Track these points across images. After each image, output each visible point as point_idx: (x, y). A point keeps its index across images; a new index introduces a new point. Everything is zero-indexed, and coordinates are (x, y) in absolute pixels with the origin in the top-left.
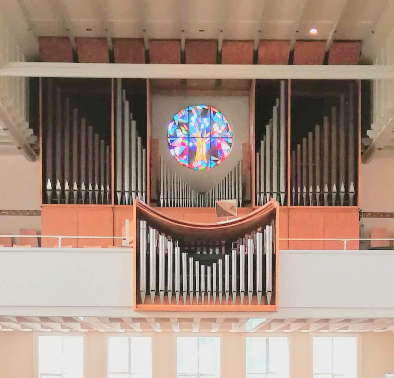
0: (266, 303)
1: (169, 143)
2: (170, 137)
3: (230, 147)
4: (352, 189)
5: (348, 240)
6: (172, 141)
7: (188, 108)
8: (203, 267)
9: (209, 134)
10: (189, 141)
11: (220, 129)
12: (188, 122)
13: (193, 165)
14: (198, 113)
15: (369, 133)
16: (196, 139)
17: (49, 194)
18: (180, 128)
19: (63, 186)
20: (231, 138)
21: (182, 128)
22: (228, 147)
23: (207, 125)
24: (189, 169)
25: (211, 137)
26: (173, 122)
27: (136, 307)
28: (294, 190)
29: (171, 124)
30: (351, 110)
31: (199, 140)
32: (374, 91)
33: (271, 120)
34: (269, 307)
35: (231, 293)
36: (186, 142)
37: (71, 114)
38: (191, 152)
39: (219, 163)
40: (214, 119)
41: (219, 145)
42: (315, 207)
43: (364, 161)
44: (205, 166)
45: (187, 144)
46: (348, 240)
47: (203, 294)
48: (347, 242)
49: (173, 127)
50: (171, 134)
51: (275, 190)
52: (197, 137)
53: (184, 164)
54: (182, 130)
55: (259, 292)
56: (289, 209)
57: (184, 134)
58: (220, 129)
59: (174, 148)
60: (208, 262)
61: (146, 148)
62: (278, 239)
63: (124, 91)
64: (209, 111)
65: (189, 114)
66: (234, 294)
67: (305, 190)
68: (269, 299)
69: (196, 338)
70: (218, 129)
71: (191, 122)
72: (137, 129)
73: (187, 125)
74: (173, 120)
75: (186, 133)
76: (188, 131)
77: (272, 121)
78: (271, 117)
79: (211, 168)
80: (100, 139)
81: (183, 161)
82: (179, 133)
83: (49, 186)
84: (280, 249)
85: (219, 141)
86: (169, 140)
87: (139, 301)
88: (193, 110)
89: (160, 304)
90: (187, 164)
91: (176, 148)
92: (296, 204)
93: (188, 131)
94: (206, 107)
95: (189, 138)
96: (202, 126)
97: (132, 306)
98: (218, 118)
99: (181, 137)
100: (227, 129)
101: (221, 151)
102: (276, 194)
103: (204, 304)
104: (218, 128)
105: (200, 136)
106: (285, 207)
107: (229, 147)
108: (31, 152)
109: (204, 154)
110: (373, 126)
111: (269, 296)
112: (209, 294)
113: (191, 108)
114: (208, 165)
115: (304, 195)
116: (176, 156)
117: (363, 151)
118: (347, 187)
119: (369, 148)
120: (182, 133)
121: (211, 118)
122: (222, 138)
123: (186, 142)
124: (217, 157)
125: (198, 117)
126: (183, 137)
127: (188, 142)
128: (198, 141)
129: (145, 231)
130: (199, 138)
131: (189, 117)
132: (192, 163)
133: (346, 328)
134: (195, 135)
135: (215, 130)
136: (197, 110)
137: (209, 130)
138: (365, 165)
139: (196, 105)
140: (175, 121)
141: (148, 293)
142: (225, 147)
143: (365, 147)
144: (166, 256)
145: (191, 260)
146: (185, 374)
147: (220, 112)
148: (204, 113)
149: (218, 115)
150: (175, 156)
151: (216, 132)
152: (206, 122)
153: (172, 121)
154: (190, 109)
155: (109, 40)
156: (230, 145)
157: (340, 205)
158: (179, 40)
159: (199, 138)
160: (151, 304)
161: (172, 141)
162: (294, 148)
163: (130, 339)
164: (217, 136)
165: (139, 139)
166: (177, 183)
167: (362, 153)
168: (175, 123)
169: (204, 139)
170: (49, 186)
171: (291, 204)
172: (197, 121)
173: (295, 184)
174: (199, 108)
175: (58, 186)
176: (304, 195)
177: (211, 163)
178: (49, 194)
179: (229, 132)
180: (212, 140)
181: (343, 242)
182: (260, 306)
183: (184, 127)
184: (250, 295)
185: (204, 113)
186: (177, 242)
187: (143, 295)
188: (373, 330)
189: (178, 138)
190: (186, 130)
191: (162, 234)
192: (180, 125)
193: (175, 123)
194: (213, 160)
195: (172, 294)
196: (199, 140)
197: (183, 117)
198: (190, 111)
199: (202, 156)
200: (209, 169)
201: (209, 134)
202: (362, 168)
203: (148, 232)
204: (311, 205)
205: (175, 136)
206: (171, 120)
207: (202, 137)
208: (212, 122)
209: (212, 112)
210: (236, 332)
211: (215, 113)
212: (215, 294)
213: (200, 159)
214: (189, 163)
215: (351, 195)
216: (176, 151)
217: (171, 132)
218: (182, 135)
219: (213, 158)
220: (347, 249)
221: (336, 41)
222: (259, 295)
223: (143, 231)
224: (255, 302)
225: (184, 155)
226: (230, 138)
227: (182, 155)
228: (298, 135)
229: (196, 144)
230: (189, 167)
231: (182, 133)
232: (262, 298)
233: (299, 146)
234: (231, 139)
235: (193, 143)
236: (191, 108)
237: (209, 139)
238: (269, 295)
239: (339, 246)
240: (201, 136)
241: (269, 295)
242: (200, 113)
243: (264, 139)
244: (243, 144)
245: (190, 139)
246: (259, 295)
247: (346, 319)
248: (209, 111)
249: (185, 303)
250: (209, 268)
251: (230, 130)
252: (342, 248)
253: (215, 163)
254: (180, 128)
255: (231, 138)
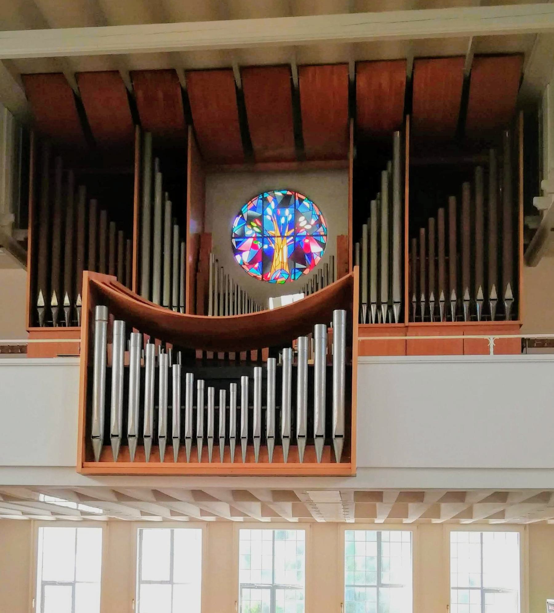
0: (333, 460)
1: (233, 246)
2: (234, 238)
3: (324, 250)
4: (509, 294)
5: (497, 337)
6: (238, 243)
7: (263, 196)
8: (211, 391)
9: (293, 230)
10: (263, 243)
11: (308, 223)
12: (263, 215)
13: (269, 276)
14: (276, 203)
15: (537, 202)
16: (273, 239)
17: (41, 312)
18: (250, 224)
19: (61, 300)
20: (324, 235)
21: (253, 224)
22: (321, 249)
23: (290, 218)
24: (263, 282)
25: (295, 235)
26: (241, 216)
27: (83, 467)
28: (414, 299)
29: (238, 219)
30: (507, 168)
31: (278, 240)
32: (544, 155)
33: (378, 193)
34: (338, 466)
35: (259, 441)
36: (259, 244)
37: (76, 191)
38: (265, 258)
39: (307, 272)
40: (300, 209)
41: (308, 246)
42: (449, 323)
43: (529, 262)
44: (286, 276)
45: (259, 247)
46: (497, 337)
47: (210, 442)
48: (496, 341)
49: (239, 224)
50: (236, 232)
51: (384, 298)
52: (275, 237)
53: (255, 275)
54: (252, 227)
55: (318, 438)
56: (407, 327)
57: (256, 232)
58: (308, 223)
59: (241, 252)
60: (220, 383)
61: (185, 241)
62: (357, 338)
63: (157, 160)
64: (293, 197)
65: (263, 204)
66: (271, 443)
67: (432, 298)
68: (339, 451)
69: (271, 531)
70: (305, 224)
71: (267, 214)
72: (173, 214)
73: (261, 219)
74: (240, 213)
75: (258, 230)
76: (262, 227)
77: (381, 195)
78: (379, 189)
79: (294, 279)
80: (118, 229)
81: (254, 271)
82: (249, 232)
83: (41, 301)
84: (359, 355)
85: (307, 241)
86: (234, 241)
87: (89, 455)
88: (270, 198)
89: (130, 462)
90: (260, 277)
91: (244, 254)
92: (418, 320)
93: (262, 227)
94: (289, 193)
95: (263, 237)
96: (283, 221)
97: (75, 465)
98: (305, 206)
99: (251, 237)
100: (319, 223)
101: (310, 255)
102: (386, 306)
103: (212, 462)
104: (305, 222)
105: (279, 235)
106: (401, 325)
107: (321, 249)
108: (18, 251)
109: (285, 260)
110: (544, 185)
111: (339, 446)
112: (222, 441)
113: (266, 195)
114: (290, 275)
115: (432, 305)
116: (244, 264)
117: (526, 243)
118: (501, 293)
119: (537, 233)
120: (253, 230)
121: (295, 208)
122: (312, 236)
123: (259, 244)
124: (305, 265)
125: (278, 206)
126: (254, 236)
127: (261, 244)
128: (276, 241)
129: (104, 324)
130: (278, 237)
131: (263, 207)
132: (268, 273)
133: (501, 515)
134: (272, 233)
135: (301, 225)
136: (275, 198)
137: (293, 225)
138: (529, 268)
139: (273, 191)
140: (243, 216)
141: (107, 441)
142: (315, 249)
143: (529, 233)
144: (143, 370)
145: (189, 377)
146: (253, 585)
147: (309, 199)
148: (286, 201)
149: (306, 203)
150: (242, 264)
151: (303, 228)
152: (288, 213)
153: (238, 216)
154: (265, 196)
155: (125, 76)
156: (323, 245)
157: (489, 319)
158: (229, 69)
159: (278, 237)
160: (112, 461)
161: (238, 243)
162: (414, 234)
163: (172, 532)
164: (304, 233)
165: (176, 228)
166: (234, 294)
167: (526, 246)
168: (243, 218)
169: (285, 238)
170: (41, 301)
171: (410, 320)
172: (275, 212)
173: (416, 289)
174: (279, 194)
175: (54, 301)
176: (432, 305)
177: (295, 273)
178: (41, 312)
179: (322, 228)
180: (297, 239)
181: (487, 341)
182: (320, 465)
183: (256, 223)
184: (302, 443)
185: (286, 201)
186: (180, 352)
187: (97, 444)
188: (546, 519)
189: (248, 238)
190: (258, 227)
191: (157, 340)
192: (250, 219)
193: (243, 218)
194: (298, 269)
195: (157, 443)
196: (278, 240)
197: (254, 209)
198: (265, 200)
199: (283, 262)
200: (292, 281)
201: (293, 230)
202: (525, 272)
203: (127, 338)
204: (443, 321)
205: (243, 236)
206: (237, 213)
207: (282, 236)
208: (296, 214)
209: (297, 199)
210: (327, 522)
211: (301, 201)
212: (233, 442)
213: (279, 268)
214: (262, 274)
215: (507, 305)
216: (246, 257)
217: (237, 231)
218: (252, 234)
219: (299, 266)
220: (495, 353)
221: (478, 56)
222: (319, 443)
223: (101, 327)
224: (310, 457)
225: (256, 263)
226: (322, 236)
227: (252, 262)
228: (419, 217)
229: (273, 245)
230: (262, 280)
231: (253, 230)
232: (323, 452)
233: (423, 230)
234: (325, 237)
235: (268, 244)
236: (266, 195)
237: (292, 238)
238: (338, 444)
239: (480, 348)
240: (281, 234)
241: (338, 444)
242: (279, 201)
243: (368, 223)
244: (338, 236)
245: (265, 239)
246: (319, 443)
247: (496, 493)
248: (293, 197)
249: (176, 459)
250: (222, 393)
251: (324, 224)
252: (486, 352)
253: (301, 273)
254: (250, 224)
255: (324, 235)
